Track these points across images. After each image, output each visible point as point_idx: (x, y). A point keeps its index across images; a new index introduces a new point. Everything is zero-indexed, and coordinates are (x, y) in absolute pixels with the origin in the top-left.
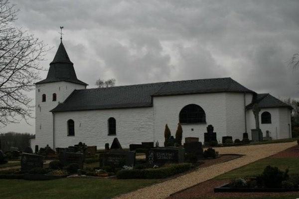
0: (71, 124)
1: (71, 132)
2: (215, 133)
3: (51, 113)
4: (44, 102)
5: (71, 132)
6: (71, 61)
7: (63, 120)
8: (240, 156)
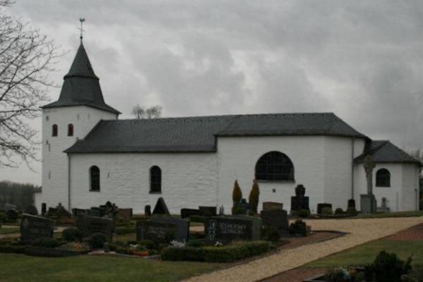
0: (95, 172)
1: (95, 186)
2: (307, 198)
3: (65, 154)
4: (55, 138)
5: (95, 186)
6: (97, 74)
7: (83, 165)
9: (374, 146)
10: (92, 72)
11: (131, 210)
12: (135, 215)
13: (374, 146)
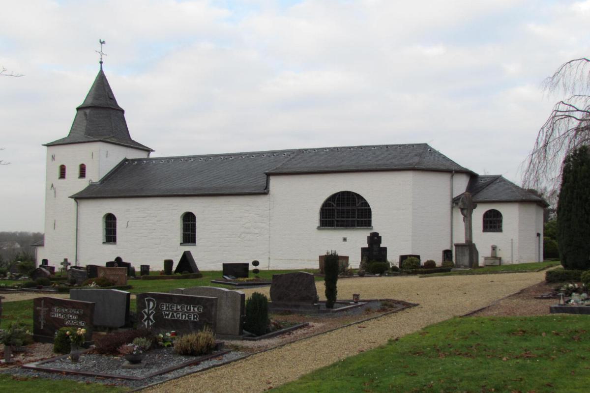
0: (110, 221)
1: (111, 236)
2: (385, 249)
3: (73, 200)
4: (62, 180)
5: (111, 236)
6: (121, 104)
7: (96, 211)
8: (406, 306)
9: (481, 182)
10: (112, 99)
11: (363, 250)
12: (152, 272)
13: (481, 182)
